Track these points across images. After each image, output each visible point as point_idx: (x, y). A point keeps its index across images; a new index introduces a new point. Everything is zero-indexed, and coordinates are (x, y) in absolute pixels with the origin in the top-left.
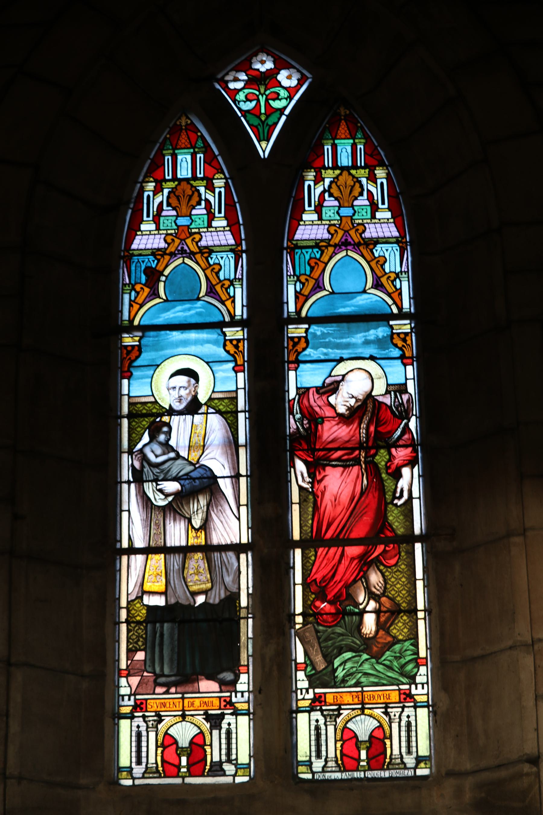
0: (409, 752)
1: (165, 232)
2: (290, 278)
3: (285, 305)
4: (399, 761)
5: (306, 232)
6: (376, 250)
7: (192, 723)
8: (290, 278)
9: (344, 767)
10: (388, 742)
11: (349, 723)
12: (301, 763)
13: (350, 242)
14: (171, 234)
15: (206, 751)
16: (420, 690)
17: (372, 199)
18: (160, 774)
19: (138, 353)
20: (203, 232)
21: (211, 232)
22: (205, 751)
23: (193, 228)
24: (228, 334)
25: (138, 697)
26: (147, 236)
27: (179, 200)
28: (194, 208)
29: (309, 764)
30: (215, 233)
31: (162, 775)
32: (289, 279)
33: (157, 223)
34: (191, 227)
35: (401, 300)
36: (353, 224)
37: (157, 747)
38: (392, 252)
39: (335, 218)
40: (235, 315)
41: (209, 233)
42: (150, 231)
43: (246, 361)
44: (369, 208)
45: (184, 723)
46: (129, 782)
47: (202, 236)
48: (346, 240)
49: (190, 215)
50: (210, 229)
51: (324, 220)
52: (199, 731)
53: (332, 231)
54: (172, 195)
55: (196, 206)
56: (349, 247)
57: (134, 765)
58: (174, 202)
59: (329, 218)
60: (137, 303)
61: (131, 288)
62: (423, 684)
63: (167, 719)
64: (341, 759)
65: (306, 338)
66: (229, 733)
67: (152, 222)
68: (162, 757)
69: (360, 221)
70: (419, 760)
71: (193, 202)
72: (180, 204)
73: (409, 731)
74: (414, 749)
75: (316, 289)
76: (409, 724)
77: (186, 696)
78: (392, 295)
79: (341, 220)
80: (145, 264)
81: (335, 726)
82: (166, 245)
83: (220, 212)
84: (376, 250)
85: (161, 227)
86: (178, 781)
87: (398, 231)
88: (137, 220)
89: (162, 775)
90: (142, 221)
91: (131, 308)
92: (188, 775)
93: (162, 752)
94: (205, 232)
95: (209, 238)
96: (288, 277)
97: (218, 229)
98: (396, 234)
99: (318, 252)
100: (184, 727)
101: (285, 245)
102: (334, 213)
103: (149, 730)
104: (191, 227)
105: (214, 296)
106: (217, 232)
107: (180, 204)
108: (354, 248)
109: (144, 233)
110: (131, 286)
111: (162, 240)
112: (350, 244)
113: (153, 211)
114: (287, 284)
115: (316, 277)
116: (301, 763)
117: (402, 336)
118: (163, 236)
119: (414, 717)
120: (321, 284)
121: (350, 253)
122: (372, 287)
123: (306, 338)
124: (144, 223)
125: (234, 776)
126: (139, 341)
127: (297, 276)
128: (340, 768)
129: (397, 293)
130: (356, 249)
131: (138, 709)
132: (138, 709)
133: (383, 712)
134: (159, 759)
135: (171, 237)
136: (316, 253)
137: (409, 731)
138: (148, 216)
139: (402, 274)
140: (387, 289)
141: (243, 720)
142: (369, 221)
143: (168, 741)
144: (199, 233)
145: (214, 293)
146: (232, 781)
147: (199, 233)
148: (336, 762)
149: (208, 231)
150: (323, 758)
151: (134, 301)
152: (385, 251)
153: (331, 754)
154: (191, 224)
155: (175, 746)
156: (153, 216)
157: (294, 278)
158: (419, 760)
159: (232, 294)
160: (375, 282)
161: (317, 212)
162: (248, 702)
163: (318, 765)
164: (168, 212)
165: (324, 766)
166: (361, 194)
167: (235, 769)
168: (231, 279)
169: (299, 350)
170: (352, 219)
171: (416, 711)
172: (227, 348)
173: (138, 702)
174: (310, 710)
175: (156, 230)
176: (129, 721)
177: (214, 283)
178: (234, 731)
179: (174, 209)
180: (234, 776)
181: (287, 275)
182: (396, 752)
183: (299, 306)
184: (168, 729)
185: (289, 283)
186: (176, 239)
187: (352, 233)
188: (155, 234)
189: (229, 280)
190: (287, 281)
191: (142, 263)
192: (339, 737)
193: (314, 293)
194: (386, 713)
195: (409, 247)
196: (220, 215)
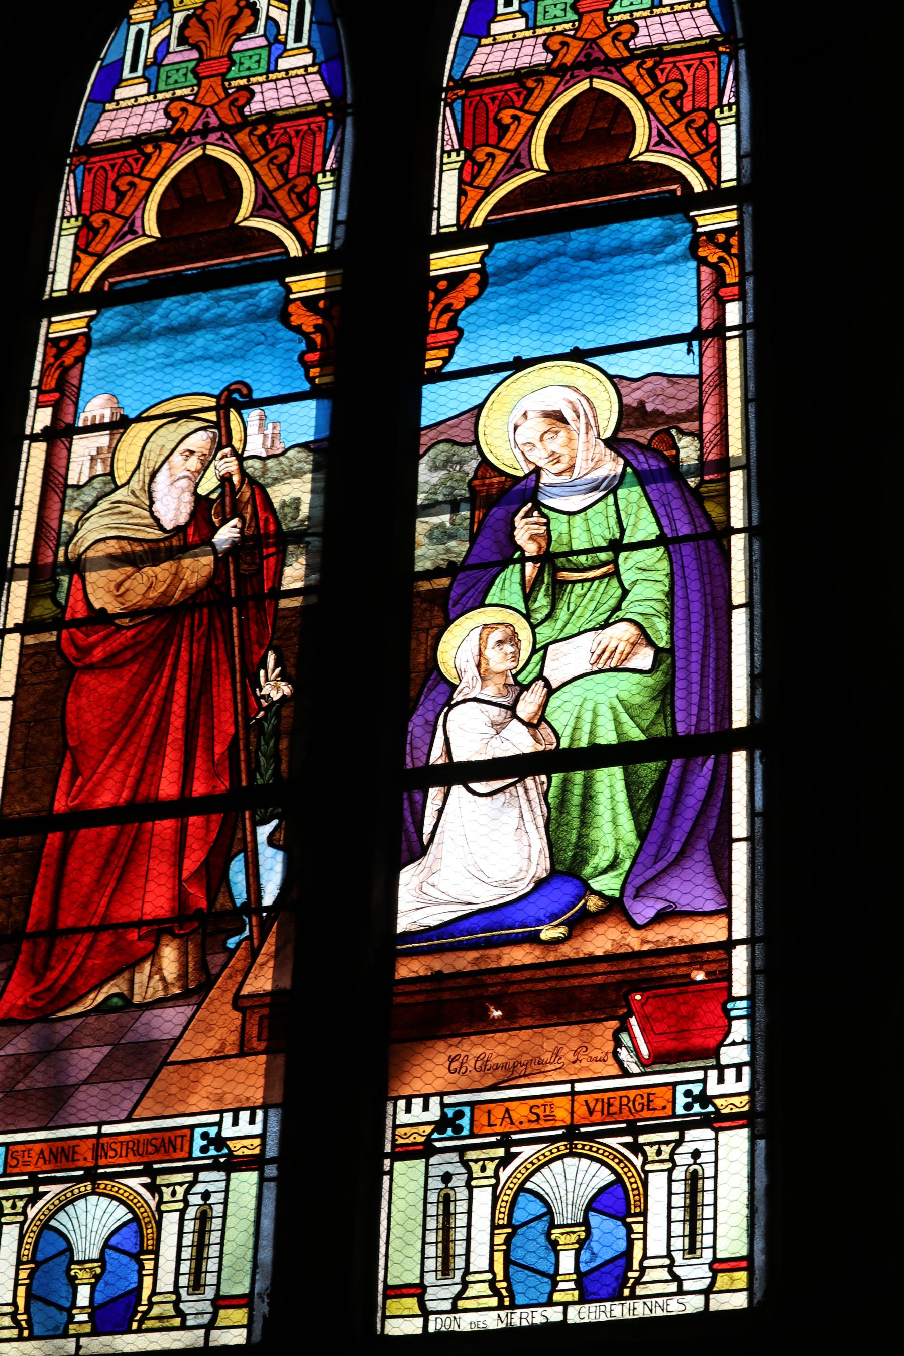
0: (197, 1285)
1: (169, 95)
2: (449, 156)
3: (435, 213)
4: (169, 1310)
5: (115, 124)
6: (662, 71)
7: (113, 1198)
8: (449, 156)
9: (30, 1327)
10: (149, 1265)
11: (61, 1216)
12: (243, 1302)
13: (598, 59)
14: (182, 98)
15: (142, 1267)
16: (730, 1085)
17: (275, 32)
18: (21, 1330)
19: (475, 291)
20: (640, 18)
21: (660, 15)
22: (630, 1231)
23: (617, 14)
24: (294, 288)
25: (448, 1100)
26: (125, 113)
27: (207, 30)
28: (238, 38)
29: (418, 1290)
30: (286, 83)
31: (507, 1302)
32: (446, 160)
33: (531, 15)
34: (229, 76)
35: (315, 233)
36: (607, 24)
37: (494, 1227)
38: (481, 105)
39: (566, 19)
40: (720, 181)
41: (272, 85)
42: (136, 98)
43: (750, 274)
44: (264, 53)
45: (93, 1199)
46: (413, 1327)
47: (637, 28)
48: (206, 124)
49: (229, 54)
50: (272, 76)
51: (541, 27)
52: (130, 1216)
53: (174, 114)
54: (193, 21)
55: (244, 34)
56: (595, 71)
57: (430, 1279)
58: (195, 33)
59: (247, 73)
60: (92, 254)
61: (462, 157)
62: (739, 1067)
63: (55, 1189)
64: (27, 1310)
65: (87, 336)
66: (694, 1180)
67: (518, 15)
68: (507, 1253)
69: (243, 82)
70: (718, 1266)
71: (240, 27)
72: (209, 38)
73: (202, 1232)
74: (211, 1279)
75: (512, 168)
76: (694, 1180)
77: (579, 1087)
78: (298, 225)
79: (580, 20)
80: (116, 169)
81: (495, 1187)
82: (550, 56)
83: (298, 38)
84: (662, 71)
85: (540, 21)
86: (554, 1314)
87: (328, 88)
88: (112, 78)
89: (507, 1302)
90: (118, 82)
91: (463, 199)
92: (576, 1299)
93: (508, 1241)
94: (645, 18)
95: (656, 28)
96: (446, 155)
97: (292, 73)
98: (713, 29)
99: (136, 160)
100: (110, 1210)
101: (445, 85)
102: (565, 10)
103: (474, 1183)
104: (611, 11)
105: (668, 149)
106: (289, 78)
107: (209, 38)
108: (222, 138)
109: (500, 39)
110: (462, 152)
111: (540, 48)
112: (214, 130)
113: (146, 58)
114: (442, 171)
115: (511, 146)
116: (243, 1302)
117: (721, 238)
118: (541, 40)
119: (711, 1157)
120: (524, 161)
121: (599, 84)
122: (252, 215)
123: (87, 336)
124: (498, 18)
125: (210, 1326)
126: (482, 261)
127: (466, 151)
128: (21, 1330)
129: (707, 155)
130: (610, 72)
131: (449, 1132)
132: (449, 1132)
133: (144, 1185)
134: (21, 1291)
135: (559, 38)
136: (710, 66)
137: (202, 1232)
138: (133, 68)
139: (722, 112)
140: (734, 143)
141: (245, 1183)
142: (261, 79)
143: (529, 1208)
144: (631, 22)
145: (668, 144)
146: (201, 1343)
147: (631, 22)
148: (492, 1283)
149: (268, 81)
150: (459, 1274)
151: (470, 184)
152: (684, 69)
153: (480, 1261)
154: (229, 70)
155: (64, 1259)
156: (146, 67)
157: (458, 155)
158: (718, 1266)
159: (712, 140)
160: (260, 202)
161: (148, 81)
162: (263, 1136)
163: (440, 1295)
164: (181, 55)
165: (459, 1296)
166: (252, 28)
167: (211, 1310)
168: (710, 107)
169: (458, 305)
170: (224, 80)
171: (228, 1180)
172: (295, 321)
173: (450, 1112)
174: (426, 1151)
175: (527, 28)
176: (420, 1164)
177: (271, 184)
178: (218, 1210)
179: (195, 46)
180: (707, 1292)
181: (443, 152)
182: (657, 1245)
183: (466, 211)
184: (527, 1179)
185: (445, 167)
186: (191, 108)
187: (606, 43)
188: (146, 104)
189: (706, 110)
190: (61, 229)
191: (667, 71)
192: (26, 1252)
193: (507, 176)
194: (153, 1188)
195: (349, 121)
196: (509, 9)
